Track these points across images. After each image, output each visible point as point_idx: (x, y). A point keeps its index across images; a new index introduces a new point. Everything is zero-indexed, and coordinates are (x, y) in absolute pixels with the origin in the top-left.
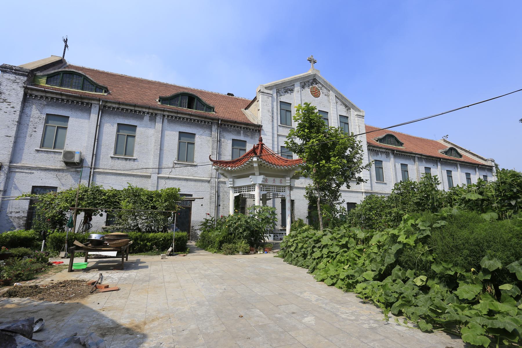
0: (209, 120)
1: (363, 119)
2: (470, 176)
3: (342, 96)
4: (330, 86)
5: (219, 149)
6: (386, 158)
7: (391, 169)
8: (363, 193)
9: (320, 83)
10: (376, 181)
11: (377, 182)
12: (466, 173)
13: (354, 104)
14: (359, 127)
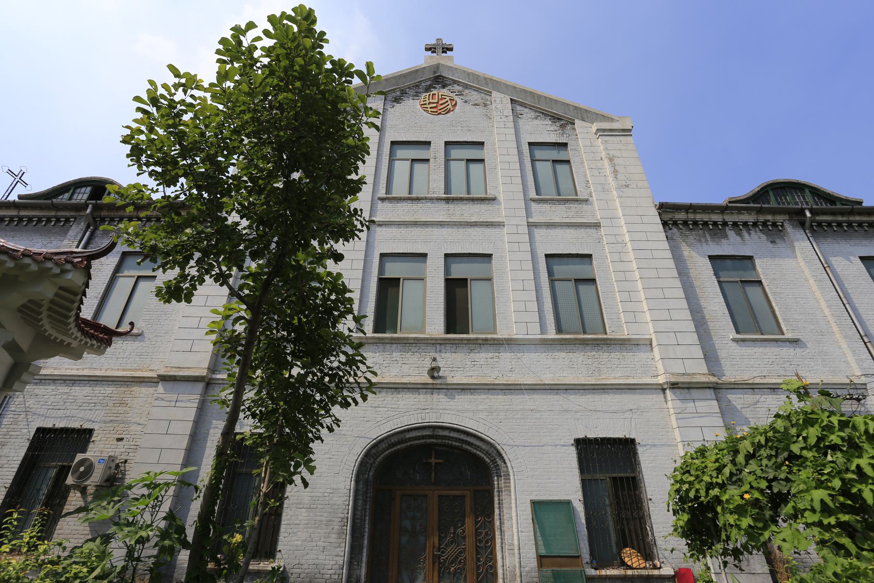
0: (68, 214)
1: (629, 138)
2: (754, 267)
3: (532, 94)
4: (488, 81)
5: (838, 284)
6: (771, 245)
7: (812, 281)
8: (664, 390)
9: (455, 82)
10: (733, 334)
11: (744, 340)
12: (711, 258)
13: (582, 106)
14: (611, 160)
